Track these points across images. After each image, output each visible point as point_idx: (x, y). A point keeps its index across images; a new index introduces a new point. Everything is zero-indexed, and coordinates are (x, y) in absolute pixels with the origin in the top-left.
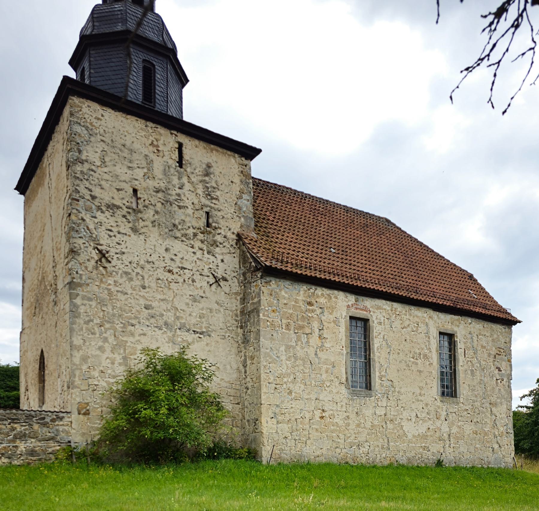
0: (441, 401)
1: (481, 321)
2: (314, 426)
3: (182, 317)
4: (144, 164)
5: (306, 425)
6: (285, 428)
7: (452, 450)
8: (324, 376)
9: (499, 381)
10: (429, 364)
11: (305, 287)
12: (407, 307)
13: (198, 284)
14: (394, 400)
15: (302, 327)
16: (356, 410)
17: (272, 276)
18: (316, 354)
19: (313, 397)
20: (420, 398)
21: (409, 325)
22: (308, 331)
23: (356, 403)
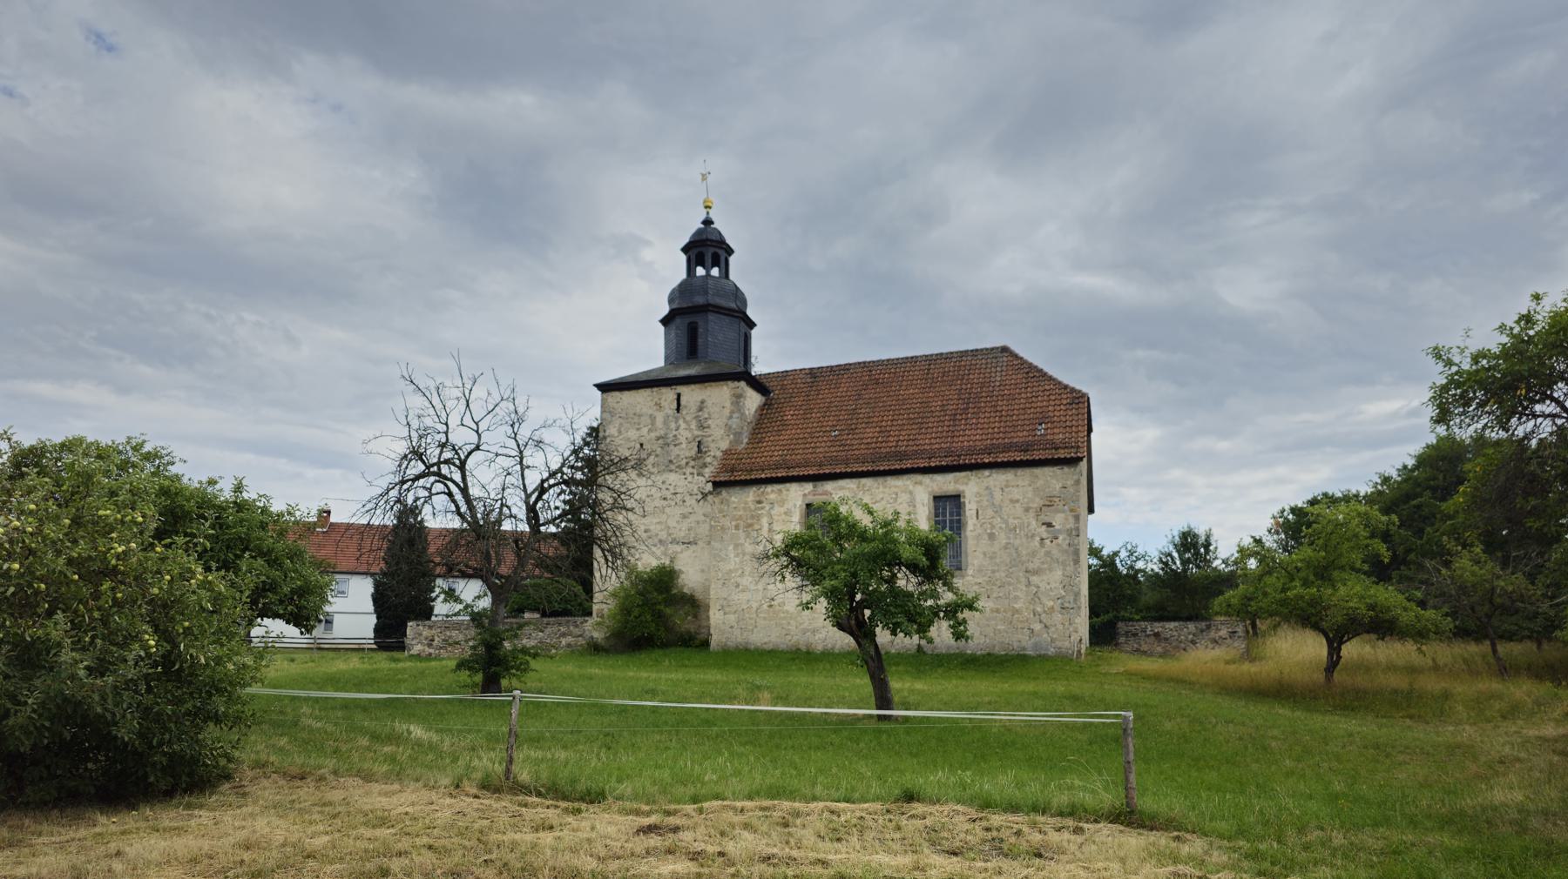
4: (649, 421)
6: (732, 618)
12: (880, 480)
13: (688, 504)
15: (751, 525)
21: (882, 499)
22: (756, 527)
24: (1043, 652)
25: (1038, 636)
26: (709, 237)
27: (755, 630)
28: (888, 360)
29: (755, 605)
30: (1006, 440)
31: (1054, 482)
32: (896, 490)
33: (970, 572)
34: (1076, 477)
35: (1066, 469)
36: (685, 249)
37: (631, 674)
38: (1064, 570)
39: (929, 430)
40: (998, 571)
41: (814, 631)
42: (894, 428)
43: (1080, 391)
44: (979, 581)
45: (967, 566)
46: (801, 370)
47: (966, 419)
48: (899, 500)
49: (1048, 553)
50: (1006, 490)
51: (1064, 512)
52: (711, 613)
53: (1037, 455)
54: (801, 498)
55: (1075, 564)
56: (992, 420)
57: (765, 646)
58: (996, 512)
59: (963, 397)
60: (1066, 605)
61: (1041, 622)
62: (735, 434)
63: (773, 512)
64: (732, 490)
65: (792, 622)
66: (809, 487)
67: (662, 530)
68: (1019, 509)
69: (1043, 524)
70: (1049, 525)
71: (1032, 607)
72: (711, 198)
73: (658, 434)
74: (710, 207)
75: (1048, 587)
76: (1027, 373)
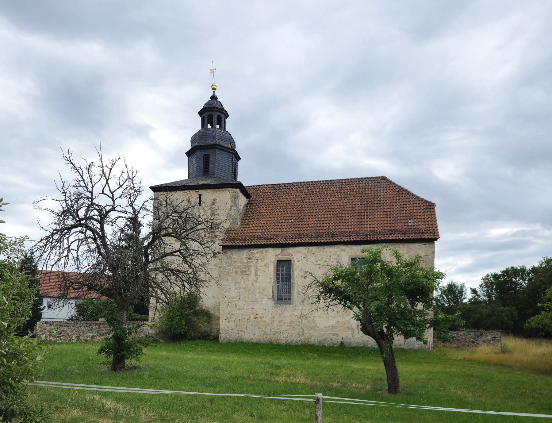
12: (321, 248)
21: (322, 258)
22: (248, 273)
24: (411, 347)
26: (216, 106)
27: (246, 331)
28: (317, 182)
29: (246, 317)
30: (392, 228)
35: (427, 245)
36: (201, 113)
37: (189, 356)
39: (346, 221)
42: (326, 219)
43: (430, 202)
46: (267, 185)
47: (367, 216)
53: (412, 237)
56: (382, 216)
57: (252, 341)
59: (363, 203)
62: (233, 219)
63: (257, 264)
64: (233, 251)
65: (268, 327)
66: (279, 250)
72: (216, 84)
76: (399, 191)
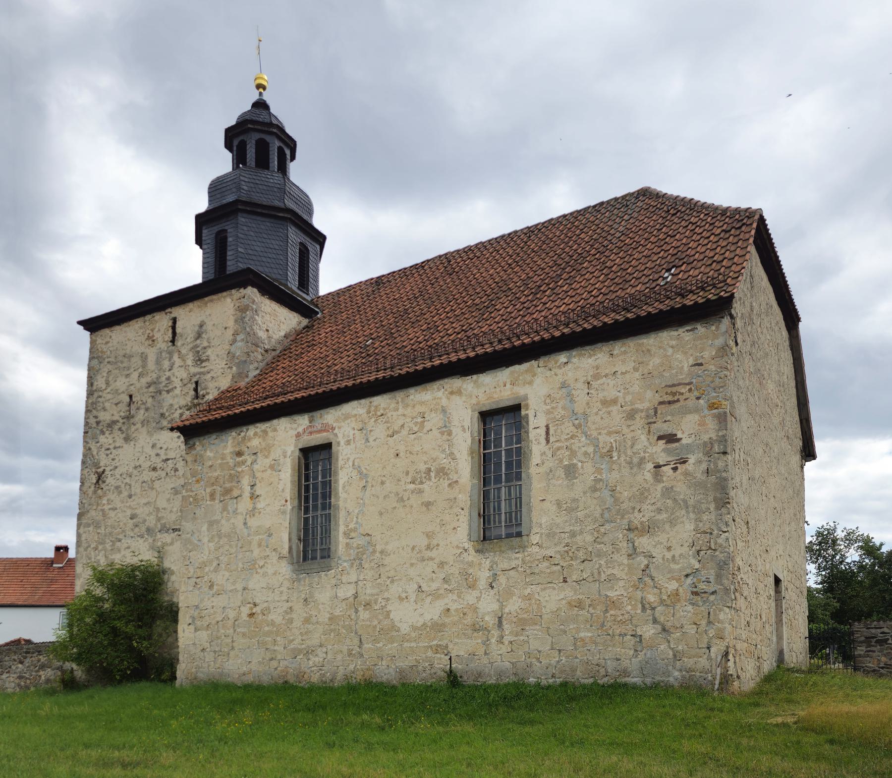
0: (477, 551)
1: (599, 345)
2: (239, 630)
3: (163, 517)
4: (140, 363)
5: (229, 629)
6: (204, 635)
7: (504, 649)
8: (256, 552)
9: (667, 470)
10: (450, 485)
11: (234, 434)
12: (400, 395)
14: (372, 568)
16: (303, 596)
17: (193, 437)
18: (245, 524)
19: (239, 586)
20: (429, 554)
21: (403, 426)
22: (235, 493)
23: (305, 585)
25: (651, 647)
27: (232, 653)
29: (232, 614)
31: (679, 356)
32: (422, 409)
33: (535, 539)
34: (719, 342)
38: (698, 520)
40: (581, 533)
41: (309, 652)
44: (549, 553)
45: (530, 528)
48: (427, 426)
49: (668, 492)
50: (595, 384)
51: (697, 410)
52: (181, 627)
54: (293, 440)
55: (718, 508)
58: (577, 427)
60: (702, 586)
61: (655, 621)
62: (238, 365)
65: (278, 639)
66: (303, 421)
67: (150, 514)
68: (617, 415)
69: (660, 438)
70: (671, 438)
71: (639, 594)
73: (149, 379)
74: (264, 88)
75: (668, 555)
